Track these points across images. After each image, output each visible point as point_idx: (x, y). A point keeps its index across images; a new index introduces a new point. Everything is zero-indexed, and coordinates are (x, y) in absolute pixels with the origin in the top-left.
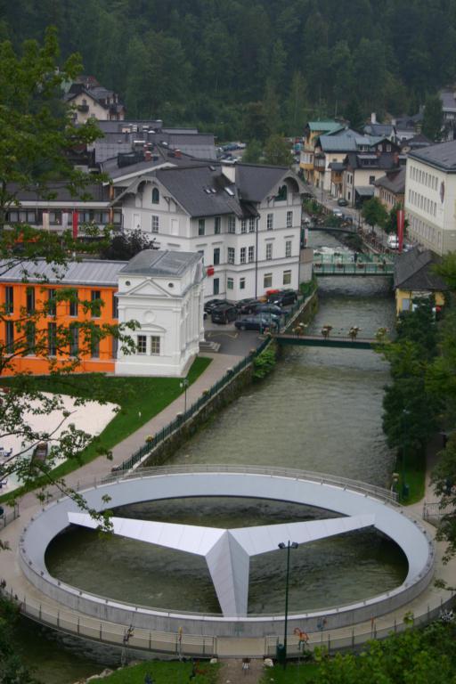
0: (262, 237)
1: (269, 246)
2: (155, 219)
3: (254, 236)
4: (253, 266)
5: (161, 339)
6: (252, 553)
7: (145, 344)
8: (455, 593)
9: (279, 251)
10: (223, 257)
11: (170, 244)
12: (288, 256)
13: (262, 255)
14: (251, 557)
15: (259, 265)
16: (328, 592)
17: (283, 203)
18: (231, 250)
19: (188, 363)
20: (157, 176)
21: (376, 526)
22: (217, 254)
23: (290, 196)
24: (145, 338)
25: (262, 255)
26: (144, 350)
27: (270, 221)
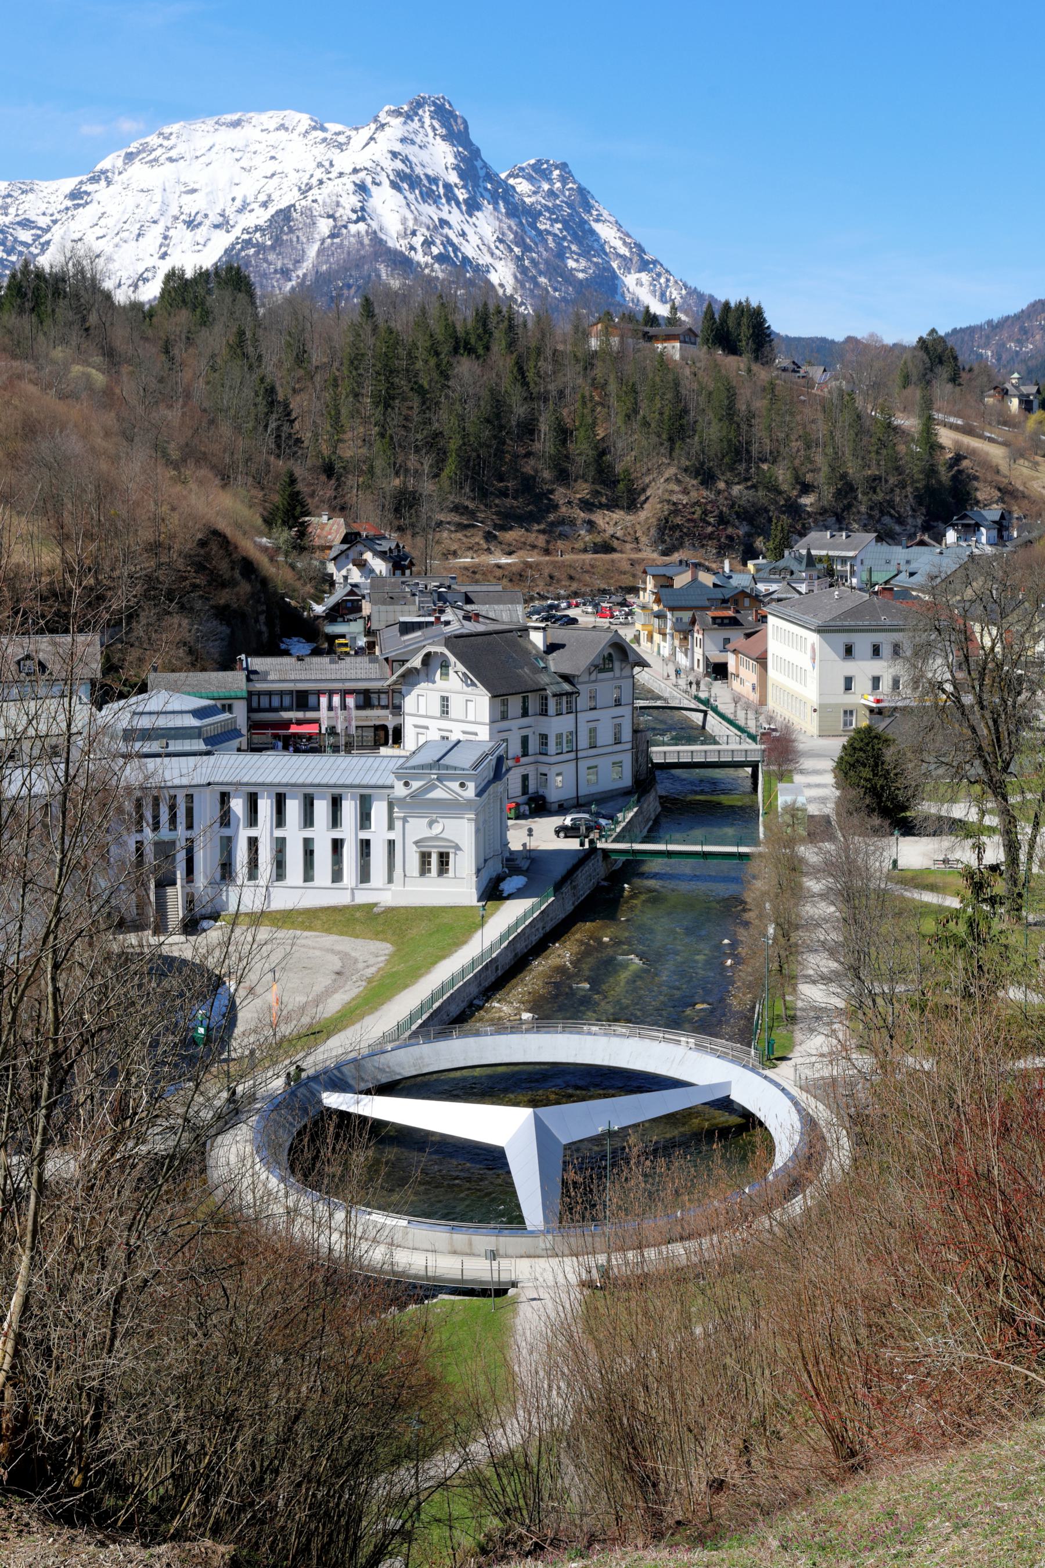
0: (583, 717)
1: (593, 731)
2: (445, 700)
3: (572, 716)
4: (572, 755)
5: (451, 856)
6: (564, 1142)
7: (429, 863)
8: (366, 1550)
9: (605, 736)
10: (533, 745)
11: (464, 732)
12: (618, 741)
13: (583, 741)
14: (568, 1147)
15: (580, 754)
16: (130, 440)
17: (609, 675)
18: (544, 737)
19: (510, 930)
20: (447, 646)
21: (767, 315)
22: (525, 741)
23: (617, 665)
24: (429, 855)
25: (583, 741)
26: (429, 870)
27: (593, 698)
